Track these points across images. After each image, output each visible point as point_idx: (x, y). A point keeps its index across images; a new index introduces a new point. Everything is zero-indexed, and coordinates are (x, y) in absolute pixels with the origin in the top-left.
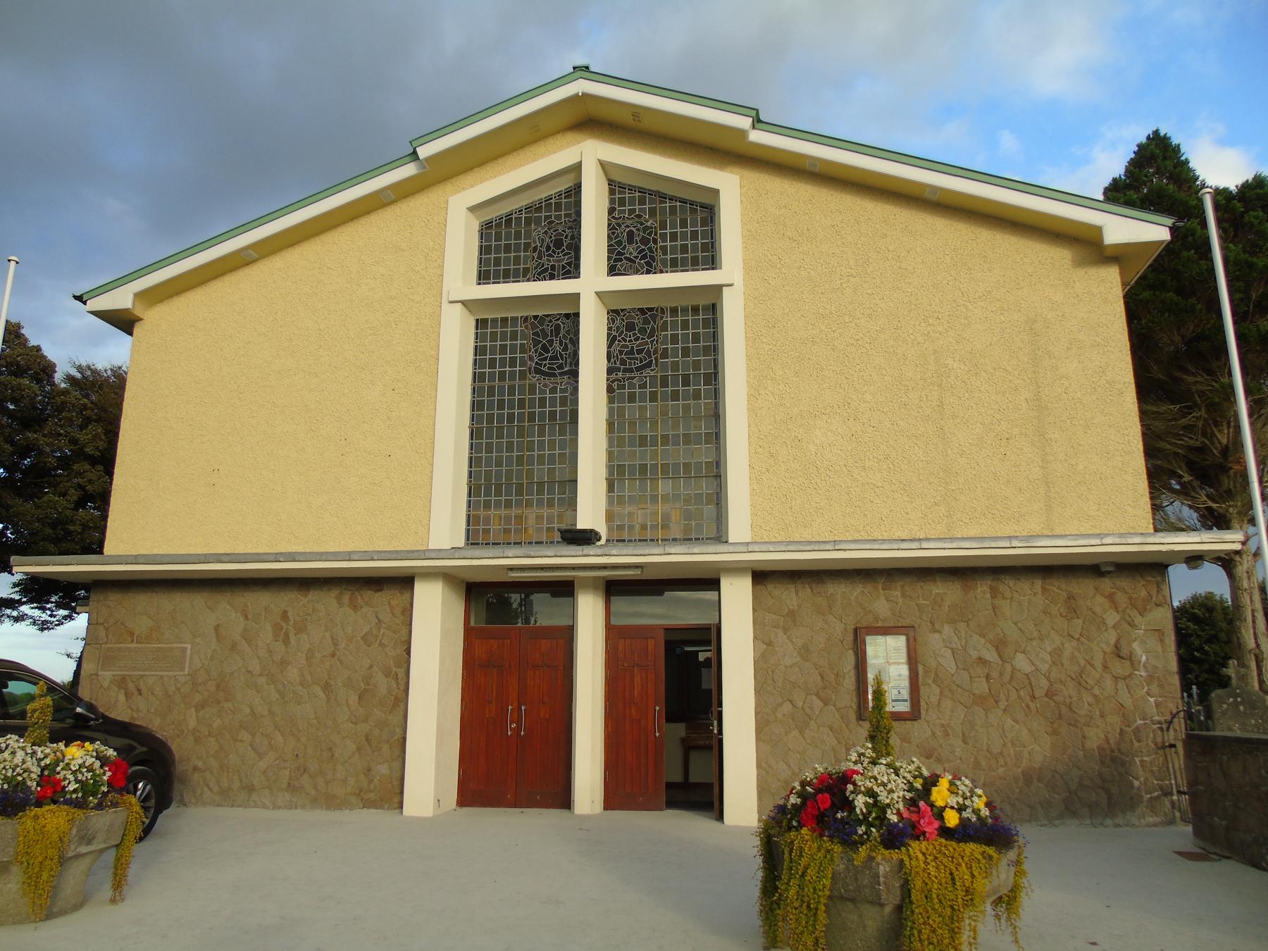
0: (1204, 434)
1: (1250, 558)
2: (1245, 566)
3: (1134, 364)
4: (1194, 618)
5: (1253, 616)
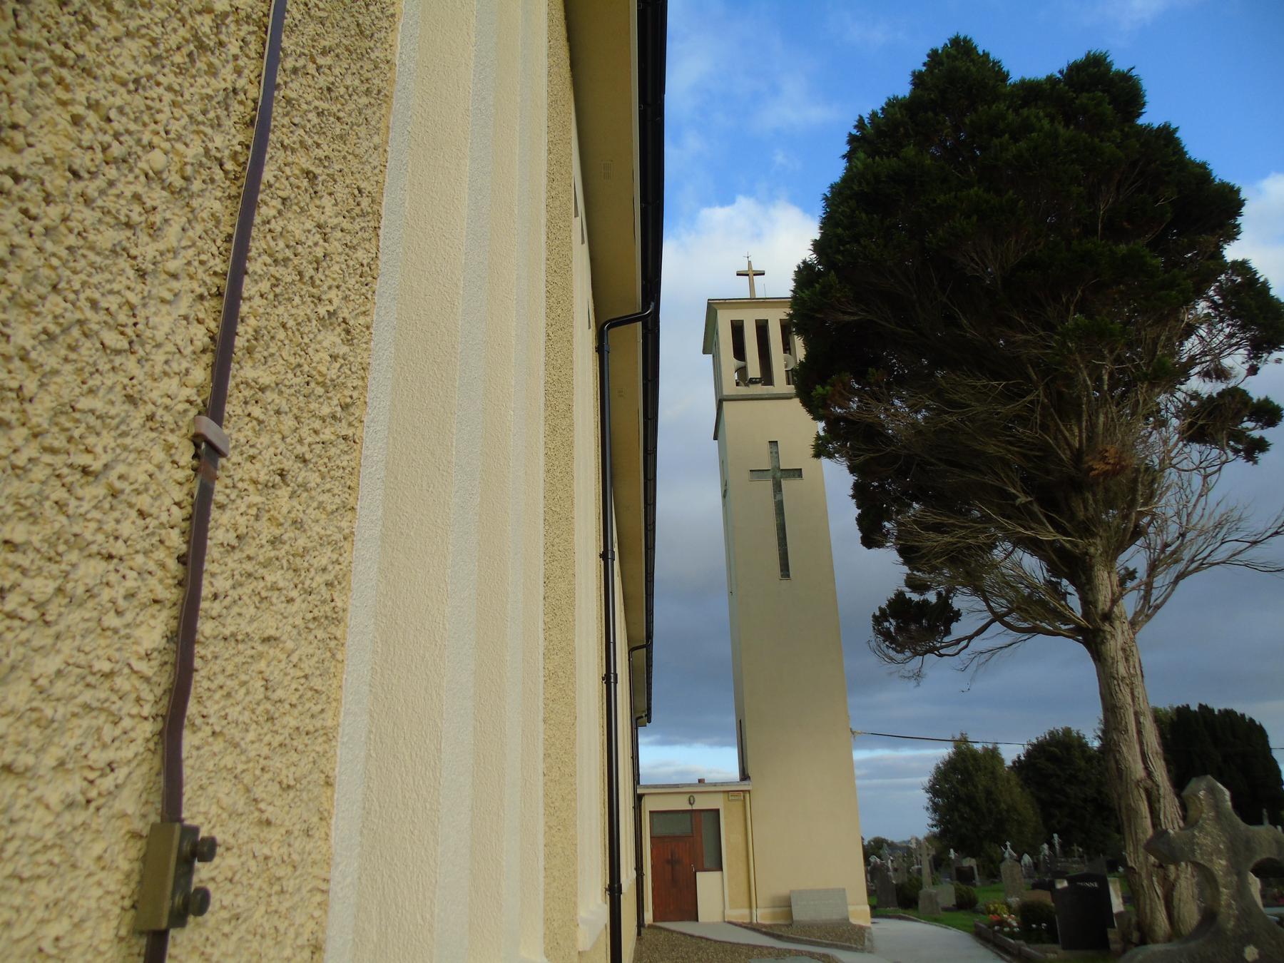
0: (1044, 427)
1: (1126, 626)
2: (1120, 639)
3: (1267, 750)
4: (1052, 758)
5: (1138, 723)
